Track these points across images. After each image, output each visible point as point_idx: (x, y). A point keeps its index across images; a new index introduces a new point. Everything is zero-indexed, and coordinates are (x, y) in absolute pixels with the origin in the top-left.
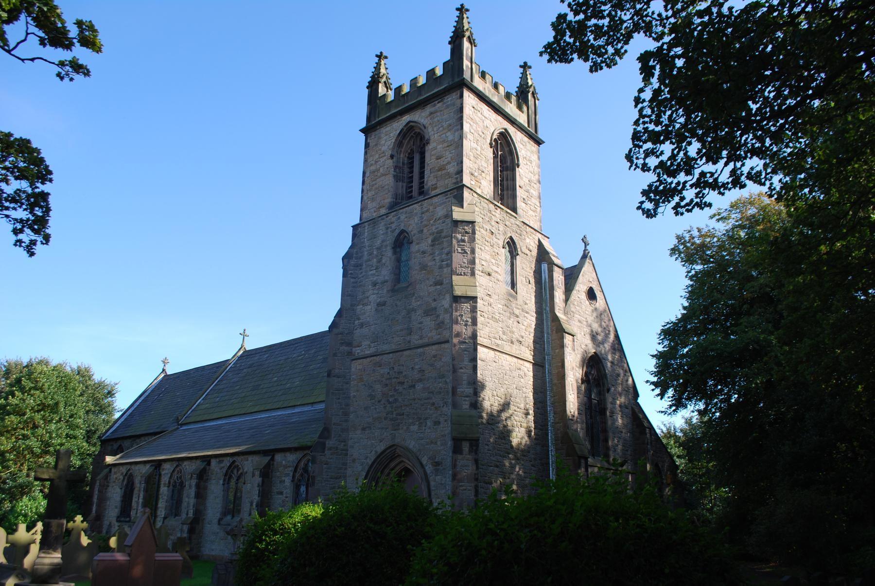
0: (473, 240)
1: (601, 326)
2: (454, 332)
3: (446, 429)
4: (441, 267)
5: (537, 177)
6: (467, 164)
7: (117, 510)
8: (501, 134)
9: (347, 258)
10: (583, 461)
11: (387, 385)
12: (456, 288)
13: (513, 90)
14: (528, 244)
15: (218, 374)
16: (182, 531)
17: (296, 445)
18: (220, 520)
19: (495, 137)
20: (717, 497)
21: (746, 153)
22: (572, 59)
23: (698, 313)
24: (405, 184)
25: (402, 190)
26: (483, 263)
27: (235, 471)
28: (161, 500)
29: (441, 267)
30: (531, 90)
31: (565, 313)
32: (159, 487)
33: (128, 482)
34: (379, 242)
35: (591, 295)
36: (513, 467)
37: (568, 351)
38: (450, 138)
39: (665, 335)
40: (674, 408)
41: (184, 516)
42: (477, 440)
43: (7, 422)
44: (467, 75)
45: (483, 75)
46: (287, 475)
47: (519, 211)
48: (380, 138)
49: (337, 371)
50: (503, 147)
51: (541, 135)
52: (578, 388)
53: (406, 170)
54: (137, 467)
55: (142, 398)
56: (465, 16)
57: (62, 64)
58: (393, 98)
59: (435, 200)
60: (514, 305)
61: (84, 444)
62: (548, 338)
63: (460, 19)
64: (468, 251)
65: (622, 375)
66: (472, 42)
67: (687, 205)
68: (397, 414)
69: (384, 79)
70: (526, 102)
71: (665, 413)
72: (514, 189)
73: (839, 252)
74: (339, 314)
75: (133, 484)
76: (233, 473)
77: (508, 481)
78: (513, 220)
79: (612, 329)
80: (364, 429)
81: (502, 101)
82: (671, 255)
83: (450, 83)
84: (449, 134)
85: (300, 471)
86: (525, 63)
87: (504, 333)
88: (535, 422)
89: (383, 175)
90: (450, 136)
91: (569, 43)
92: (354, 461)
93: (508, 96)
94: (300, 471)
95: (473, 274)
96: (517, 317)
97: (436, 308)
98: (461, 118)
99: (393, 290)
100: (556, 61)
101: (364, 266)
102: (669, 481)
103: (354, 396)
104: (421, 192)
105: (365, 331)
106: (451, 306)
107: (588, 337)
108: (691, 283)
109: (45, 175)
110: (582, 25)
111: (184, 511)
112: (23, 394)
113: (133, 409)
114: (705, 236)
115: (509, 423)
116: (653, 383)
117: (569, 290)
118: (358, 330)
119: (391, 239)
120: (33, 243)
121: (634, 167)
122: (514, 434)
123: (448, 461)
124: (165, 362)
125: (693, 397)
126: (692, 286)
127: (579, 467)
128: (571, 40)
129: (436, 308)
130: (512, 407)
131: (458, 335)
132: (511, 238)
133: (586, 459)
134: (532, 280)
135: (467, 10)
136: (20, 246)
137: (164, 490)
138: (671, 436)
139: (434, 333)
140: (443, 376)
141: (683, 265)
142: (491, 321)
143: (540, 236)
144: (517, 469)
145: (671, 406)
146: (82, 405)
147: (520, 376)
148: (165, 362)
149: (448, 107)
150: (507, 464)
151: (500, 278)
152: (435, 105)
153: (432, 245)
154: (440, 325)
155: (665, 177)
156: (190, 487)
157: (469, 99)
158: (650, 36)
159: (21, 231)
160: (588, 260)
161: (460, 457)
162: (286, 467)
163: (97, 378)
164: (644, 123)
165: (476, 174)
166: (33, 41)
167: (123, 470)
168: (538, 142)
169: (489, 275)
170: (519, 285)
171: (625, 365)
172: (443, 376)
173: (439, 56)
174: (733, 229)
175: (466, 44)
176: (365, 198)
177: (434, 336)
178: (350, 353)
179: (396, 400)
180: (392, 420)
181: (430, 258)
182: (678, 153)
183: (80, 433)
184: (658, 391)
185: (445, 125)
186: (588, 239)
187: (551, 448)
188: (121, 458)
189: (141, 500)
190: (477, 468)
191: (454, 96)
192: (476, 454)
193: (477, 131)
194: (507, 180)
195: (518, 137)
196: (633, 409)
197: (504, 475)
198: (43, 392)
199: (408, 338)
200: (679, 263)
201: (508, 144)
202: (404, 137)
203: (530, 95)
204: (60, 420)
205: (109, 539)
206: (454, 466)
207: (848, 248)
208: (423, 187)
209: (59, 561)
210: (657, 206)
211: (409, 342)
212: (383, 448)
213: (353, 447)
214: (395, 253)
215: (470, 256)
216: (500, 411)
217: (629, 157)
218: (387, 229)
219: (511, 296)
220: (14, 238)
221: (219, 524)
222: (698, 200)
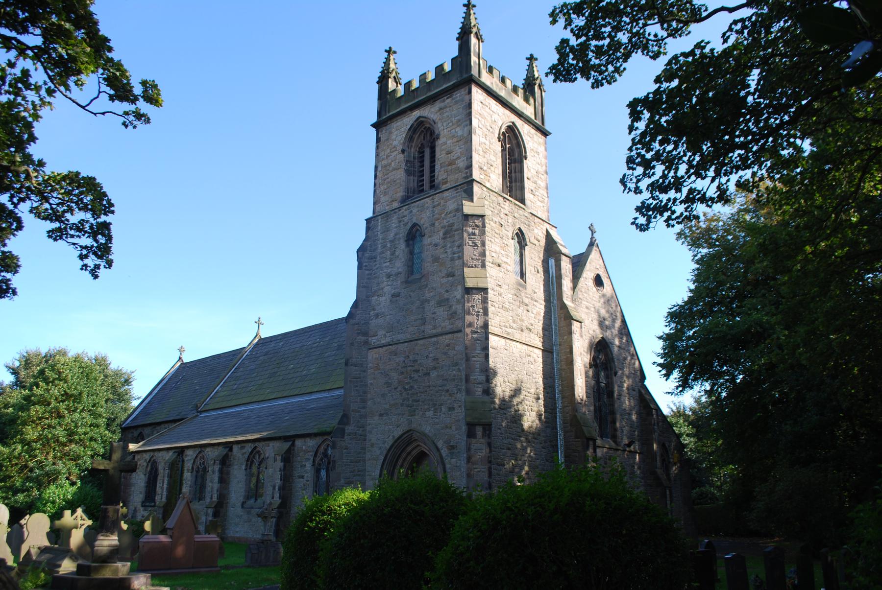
0: (483, 233)
1: (608, 312)
2: (467, 322)
3: (460, 413)
4: (452, 259)
5: (544, 168)
6: (476, 159)
7: (141, 496)
8: (509, 127)
9: (361, 251)
10: (591, 443)
11: (402, 373)
12: (467, 279)
13: (520, 83)
14: (536, 235)
15: (235, 362)
16: (207, 515)
17: (315, 431)
18: (243, 503)
19: (503, 130)
20: (725, 473)
21: (732, 168)
22: (576, 79)
23: (704, 295)
24: (416, 178)
25: (413, 184)
26: (494, 254)
27: (257, 456)
28: (184, 486)
29: (452, 259)
30: (538, 82)
31: (573, 301)
32: (182, 473)
33: (152, 469)
34: (392, 235)
35: (598, 281)
36: (524, 449)
37: (576, 337)
38: (460, 133)
39: (672, 318)
40: (680, 389)
41: (208, 500)
42: (489, 425)
43: (33, 413)
44: (474, 72)
45: (490, 70)
46: (308, 459)
47: (527, 202)
48: (391, 133)
49: (354, 360)
50: (511, 140)
51: (547, 127)
52: (586, 373)
53: (417, 164)
54: (160, 454)
55: (160, 386)
56: (472, 12)
57: (126, 113)
58: (402, 93)
59: (446, 194)
60: (523, 294)
61: (107, 432)
62: (556, 329)
63: (467, 15)
64: (479, 243)
65: (629, 358)
66: (479, 37)
67: (678, 217)
68: (413, 401)
69: (394, 74)
70: (533, 94)
71: (672, 393)
72: (522, 181)
73: (823, 251)
74: (355, 305)
75: (157, 470)
76: (254, 458)
77: (520, 462)
78: (521, 212)
79: (619, 314)
80: (381, 415)
81: (509, 94)
82: (677, 239)
83: (458, 79)
84: (458, 129)
85: (320, 456)
86: (532, 55)
87: (514, 322)
88: (545, 407)
89: (394, 169)
90: (459, 132)
91: (572, 65)
92: (372, 445)
93: (515, 89)
94: (320, 456)
95: (484, 266)
96: (527, 305)
97: (448, 299)
98: (470, 114)
99: (407, 282)
100: (561, 81)
101: (378, 258)
102: (676, 460)
103: (372, 384)
104: (432, 186)
105: (380, 321)
106: (463, 297)
107: (596, 323)
108: (697, 266)
109: (108, 209)
110: (584, 47)
111: (208, 496)
112: (47, 384)
113: (151, 397)
114: (711, 220)
115: (520, 407)
116: (660, 365)
117: (576, 276)
118: (374, 321)
119: (403, 232)
120: (97, 267)
121: (627, 190)
122: (525, 418)
123: (463, 445)
124: (181, 350)
125: (699, 378)
126: (698, 269)
127: (588, 449)
128: (575, 62)
129: (448, 299)
130: (523, 393)
131: (470, 325)
132: (520, 229)
133: (594, 440)
134: (541, 270)
135: (474, 6)
136: (86, 270)
137: (187, 475)
138: (680, 415)
139: (447, 323)
140: (456, 364)
141: (690, 249)
142: (501, 311)
143: (548, 226)
144: (529, 451)
145: (677, 387)
146: (104, 393)
147: (530, 363)
148: (181, 350)
149: (456, 102)
150: (519, 446)
151: (509, 268)
152: (444, 101)
153: (444, 239)
154: (453, 315)
155: (657, 193)
156: (213, 472)
157: (477, 94)
158: (647, 55)
159: (86, 256)
160: (595, 248)
161: (474, 441)
162: (306, 452)
163: (113, 366)
164: (637, 149)
165: (485, 168)
166: (104, 97)
167: (147, 456)
168: (545, 134)
169: (499, 266)
170: (528, 275)
171: (632, 349)
172: (456, 364)
173: (446, 52)
174: (738, 213)
175: (473, 40)
176: (378, 192)
177: (447, 325)
178: (366, 343)
179: (412, 387)
180: (408, 406)
181: (442, 250)
182: (669, 172)
183: (102, 421)
184: (664, 372)
185: (454, 120)
186: (596, 227)
187: (560, 432)
188: (143, 445)
189: (165, 486)
190: (491, 451)
191: (463, 91)
192: (489, 437)
193: (485, 126)
194: (515, 172)
195: (525, 130)
196: (640, 392)
197: (515, 457)
198: (66, 382)
199: (422, 328)
200: (685, 248)
201: (515, 135)
202: (414, 132)
203: (536, 87)
204: (83, 411)
205: (144, 523)
206: (469, 449)
207: (831, 249)
208: (434, 181)
209: (116, 543)
210: (649, 221)
211: (423, 331)
212: (400, 433)
213: (370, 432)
214: (408, 245)
215: (480, 249)
216: (512, 397)
217: (623, 182)
218: (400, 222)
219: (520, 285)
220: (81, 263)
221: (243, 507)
222: (687, 214)
